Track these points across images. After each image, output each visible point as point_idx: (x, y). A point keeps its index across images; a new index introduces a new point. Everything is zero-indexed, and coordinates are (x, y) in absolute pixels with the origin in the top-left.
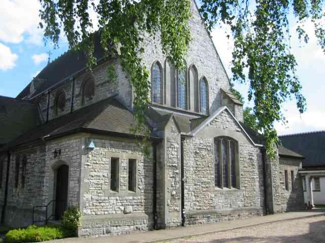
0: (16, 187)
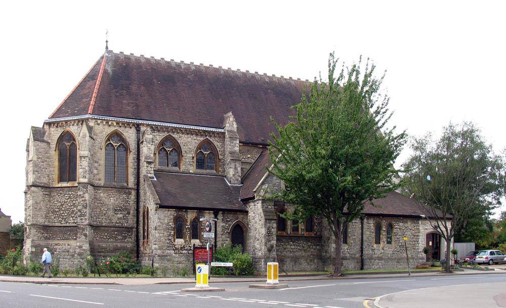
0: (378, 241)
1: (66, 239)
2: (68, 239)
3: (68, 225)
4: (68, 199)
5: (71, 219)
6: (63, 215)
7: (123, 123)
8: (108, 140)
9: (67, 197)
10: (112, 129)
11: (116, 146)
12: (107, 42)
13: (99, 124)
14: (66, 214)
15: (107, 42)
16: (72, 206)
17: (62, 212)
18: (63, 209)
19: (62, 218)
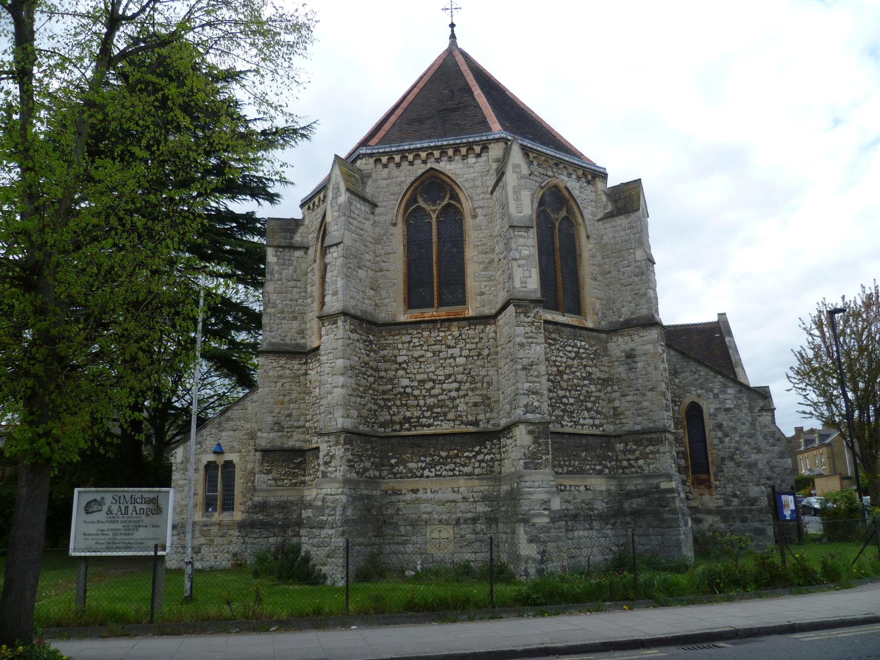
1: (578, 473)
2: (581, 472)
3: (579, 430)
4: (574, 359)
5: (586, 414)
6: (565, 400)
7: (443, 150)
8: (413, 200)
9: (570, 352)
10: (419, 169)
11: (434, 211)
12: (452, 25)
13: (385, 166)
14: (572, 401)
15: (452, 25)
16: (584, 379)
17: (561, 393)
18: (564, 385)
19: (564, 411)
